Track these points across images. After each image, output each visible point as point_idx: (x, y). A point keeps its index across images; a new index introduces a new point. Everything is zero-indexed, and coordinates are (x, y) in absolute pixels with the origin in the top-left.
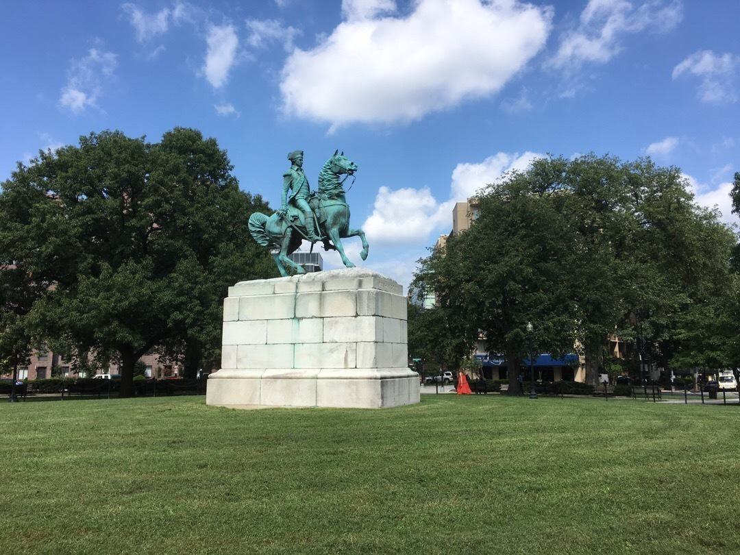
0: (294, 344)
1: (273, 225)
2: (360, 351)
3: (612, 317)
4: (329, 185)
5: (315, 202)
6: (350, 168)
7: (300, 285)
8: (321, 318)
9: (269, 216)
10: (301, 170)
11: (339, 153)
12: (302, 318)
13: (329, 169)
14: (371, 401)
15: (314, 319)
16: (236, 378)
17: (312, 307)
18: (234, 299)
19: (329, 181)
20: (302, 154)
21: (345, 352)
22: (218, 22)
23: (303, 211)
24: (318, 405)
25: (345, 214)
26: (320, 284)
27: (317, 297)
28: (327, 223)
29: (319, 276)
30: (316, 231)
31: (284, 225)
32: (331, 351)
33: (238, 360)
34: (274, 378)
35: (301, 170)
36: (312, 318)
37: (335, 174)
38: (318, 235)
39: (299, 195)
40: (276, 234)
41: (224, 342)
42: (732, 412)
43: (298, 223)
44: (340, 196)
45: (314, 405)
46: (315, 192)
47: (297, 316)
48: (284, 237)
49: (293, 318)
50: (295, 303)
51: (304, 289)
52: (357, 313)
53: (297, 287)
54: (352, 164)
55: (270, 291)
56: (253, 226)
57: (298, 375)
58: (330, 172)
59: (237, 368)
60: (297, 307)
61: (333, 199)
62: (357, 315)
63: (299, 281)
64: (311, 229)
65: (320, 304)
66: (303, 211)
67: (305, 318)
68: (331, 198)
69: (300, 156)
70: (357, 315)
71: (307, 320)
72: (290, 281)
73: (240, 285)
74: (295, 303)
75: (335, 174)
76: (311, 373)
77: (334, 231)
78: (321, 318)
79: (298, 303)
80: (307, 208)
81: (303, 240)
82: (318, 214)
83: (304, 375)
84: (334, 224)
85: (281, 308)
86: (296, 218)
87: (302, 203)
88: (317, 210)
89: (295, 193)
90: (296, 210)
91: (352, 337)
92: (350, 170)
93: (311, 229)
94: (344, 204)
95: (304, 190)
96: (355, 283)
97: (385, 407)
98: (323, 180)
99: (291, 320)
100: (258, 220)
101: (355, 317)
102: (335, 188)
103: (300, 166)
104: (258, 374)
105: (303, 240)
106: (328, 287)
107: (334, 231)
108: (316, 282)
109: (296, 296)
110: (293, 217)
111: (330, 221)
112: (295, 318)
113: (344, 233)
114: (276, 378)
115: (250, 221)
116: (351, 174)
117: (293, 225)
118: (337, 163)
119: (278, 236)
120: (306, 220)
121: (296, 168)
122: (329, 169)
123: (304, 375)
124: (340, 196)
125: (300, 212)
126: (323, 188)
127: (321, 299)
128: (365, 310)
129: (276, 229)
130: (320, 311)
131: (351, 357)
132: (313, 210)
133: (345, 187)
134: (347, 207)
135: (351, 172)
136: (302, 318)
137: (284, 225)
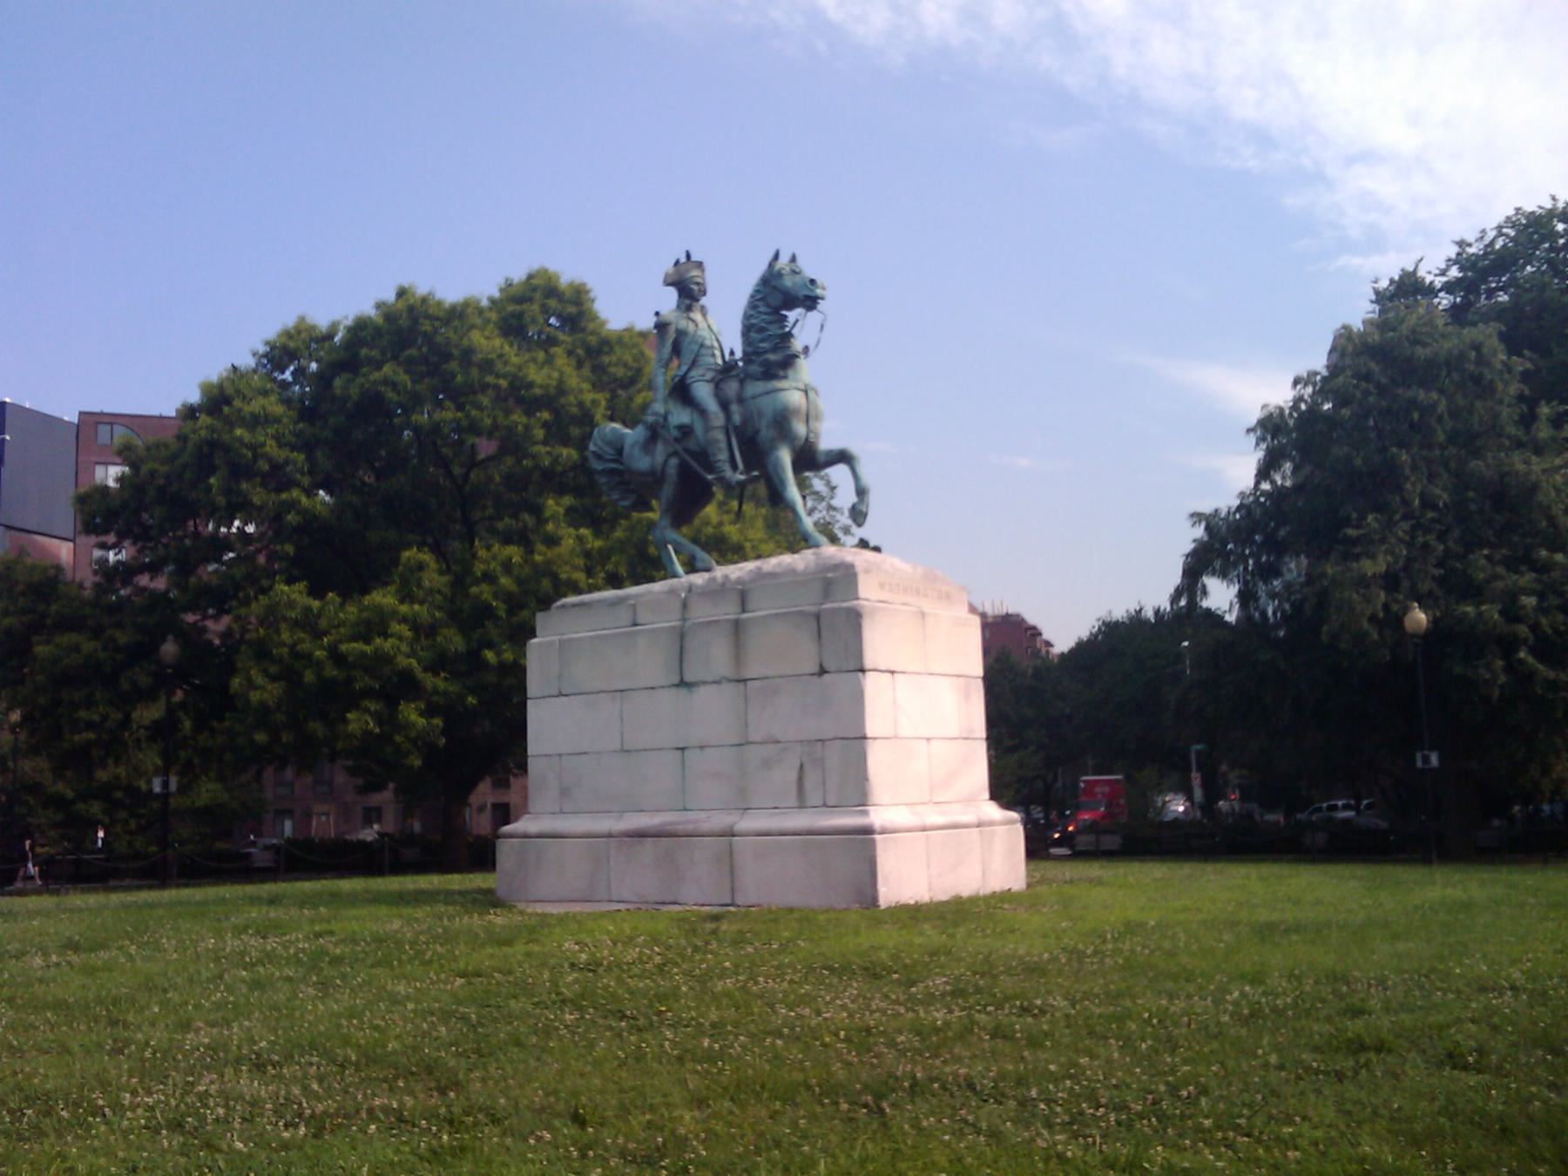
0: (683, 749)
1: (636, 452)
4: (762, 341)
8: (739, 681)
9: (687, 573)
17: (714, 656)
18: (551, 644)
31: (660, 450)
32: (767, 764)
33: (565, 792)
34: (683, 770)
43: (691, 444)
51: (701, 612)
56: (598, 457)
57: (689, 827)
58: (762, 309)
59: (562, 812)
62: (823, 671)
67: (704, 683)
71: (806, 672)
76: (719, 821)
78: (678, 749)
80: (712, 405)
82: (737, 419)
85: (650, 664)
86: (686, 431)
97: (597, 477)
99: (674, 690)
114: (641, 834)
115: (592, 447)
123: (705, 827)
125: (696, 416)
129: (642, 463)
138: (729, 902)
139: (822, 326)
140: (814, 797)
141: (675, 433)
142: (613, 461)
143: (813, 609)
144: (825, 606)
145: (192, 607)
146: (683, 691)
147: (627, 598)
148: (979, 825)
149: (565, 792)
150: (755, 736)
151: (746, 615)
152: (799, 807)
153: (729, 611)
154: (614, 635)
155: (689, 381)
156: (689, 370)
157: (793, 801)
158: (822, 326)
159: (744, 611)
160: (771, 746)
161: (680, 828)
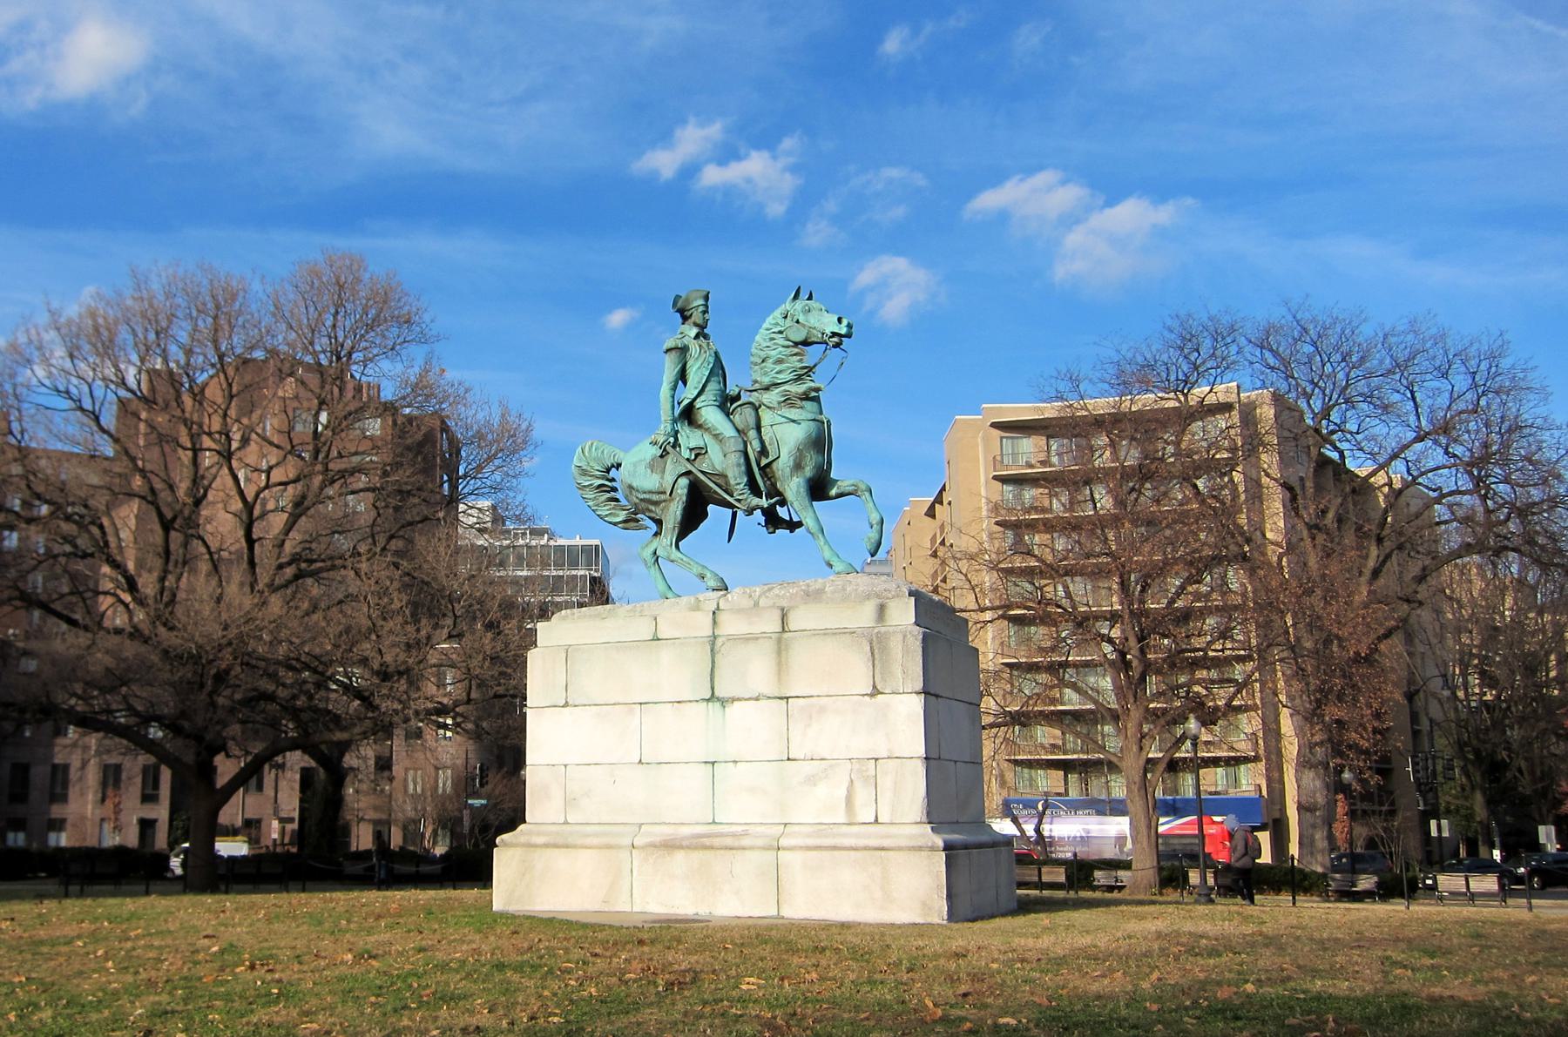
0: (713, 763)
1: (642, 469)
2: (886, 782)
5: (744, 417)
10: (706, 337)
11: (804, 295)
12: (733, 700)
13: (781, 332)
14: (924, 904)
15: (763, 702)
19: (779, 361)
20: (706, 298)
21: (846, 784)
24: (782, 914)
26: (777, 615)
27: (768, 646)
32: (811, 780)
35: (706, 337)
36: (757, 699)
38: (758, 493)
39: (702, 398)
40: (651, 492)
41: (530, 757)
42: (1261, 742)
45: (774, 913)
47: (717, 693)
49: (708, 700)
50: (713, 662)
52: (874, 687)
53: (715, 622)
61: (792, 406)
62: (875, 692)
63: (718, 608)
65: (779, 664)
67: (738, 699)
68: (788, 401)
70: (875, 692)
73: (1122, 912)
74: (713, 662)
77: (794, 488)
79: (718, 658)
80: (728, 431)
81: (711, 508)
86: (699, 452)
90: (698, 433)
91: (862, 745)
92: (834, 334)
95: (713, 387)
96: (869, 609)
101: (872, 695)
102: (799, 378)
105: (711, 508)
106: (793, 624)
107: (794, 488)
108: (764, 608)
110: (691, 450)
112: (713, 698)
113: (819, 488)
119: (655, 497)
120: (722, 460)
122: (781, 332)
125: (708, 438)
127: (779, 652)
128: (897, 679)
129: (648, 481)
130: (779, 680)
131: (863, 795)
136: (733, 700)
137: (672, 468)
141: (686, 454)
156: (699, 394)
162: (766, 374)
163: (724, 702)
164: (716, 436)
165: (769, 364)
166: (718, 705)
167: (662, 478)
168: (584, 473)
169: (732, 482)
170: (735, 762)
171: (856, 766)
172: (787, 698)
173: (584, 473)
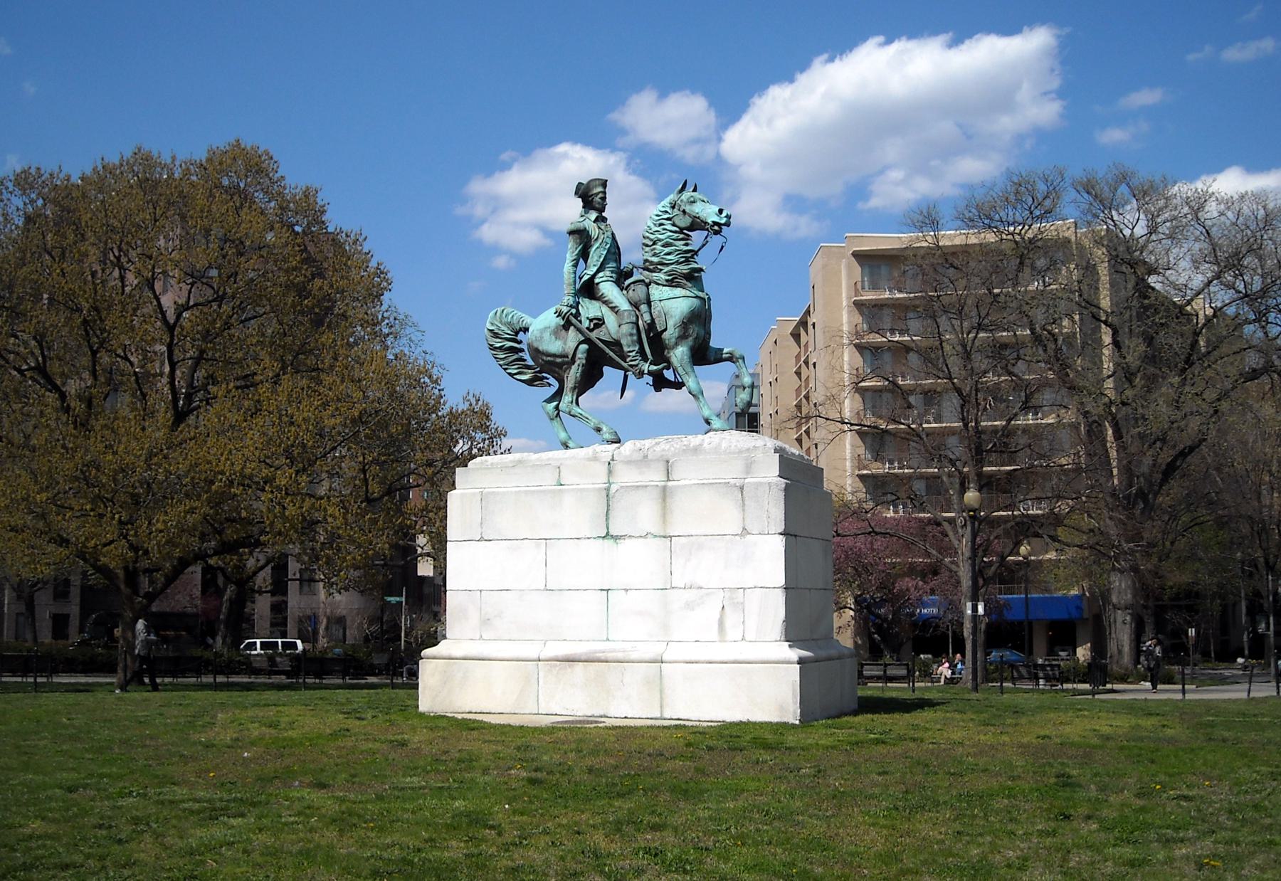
0: (608, 590)
1: (547, 335)
3: (1109, 814)
4: (669, 254)
6: (716, 219)
7: (618, 468)
8: (664, 537)
13: (668, 219)
15: (650, 540)
16: (607, 662)
20: (604, 184)
22: (619, 102)
23: (614, 309)
25: (699, 319)
26: (662, 466)
28: (666, 335)
29: (658, 449)
30: (642, 352)
32: (689, 606)
33: (486, 622)
35: (604, 220)
36: (645, 537)
37: (681, 231)
38: (645, 359)
39: (601, 274)
44: (693, 277)
46: (634, 267)
47: (612, 532)
48: (573, 361)
50: (608, 506)
51: (625, 476)
52: (744, 529)
53: (610, 472)
54: (721, 211)
55: (548, 479)
57: (620, 656)
60: (612, 514)
62: (745, 532)
63: (613, 460)
64: (629, 346)
66: (614, 309)
68: (671, 283)
69: (600, 189)
70: (745, 532)
71: (633, 540)
72: (595, 458)
74: (608, 506)
75: (681, 231)
77: (679, 354)
81: (606, 369)
83: (634, 656)
84: (682, 337)
86: (599, 323)
87: (608, 288)
88: (644, 308)
89: (595, 269)
90: (596, 304)
92: (715, 223)
93: (629, 346)
94: (700, 294)
98: (654, 243)
99: (601, 539)
100: (509, 324)
101: (741, 535)
103: (601, 210)
104: (531, 651)
105: (606, 369)
108: (651, 460)
109: (608, 489)
110: (591, 320)
111: (670, 334)
113: (703, 355)
116: (717, 233)
117: (593, 335)
118: (688, 209)
119: (559, 360)
121: (593, 215)
122: (668, 219)
124: (693, 277)
125: (605, 309)
126: (655, 259)
131: (732, 619)
132: (636, 305)
133: (701, 261)
134: (705, 302)
135: (717, 229)
138: (659, 716)
139: (722, 247)
140: (733, 632)
141: (586, 324)
142: (572, 324)
143: (739, 482)
144: (747, 481)
145: (80, 478)
146: (609, 542)
147: (8, 604)
148: (839, 658)
149: (486, 622)
150: (677, 582)
151: (670, 484)
152: (720, 641)
153: (655, 476)
154: (534, 491)
155: (597, 281)
157: (714, 633)
158: (722, 247)
159: (668, 480)
160: (694, 591)
161: (610, 656)
162: (654, 255)
163: (616, 538)
164: (612, 308)
165: (658, 247)
166: (612, 541)
167: (565, 344)
168: (496, 335)
169: (626, 349)
170: (626, 590)
171: (728, 594)
172: (671, 537)
173: (496, 335)
